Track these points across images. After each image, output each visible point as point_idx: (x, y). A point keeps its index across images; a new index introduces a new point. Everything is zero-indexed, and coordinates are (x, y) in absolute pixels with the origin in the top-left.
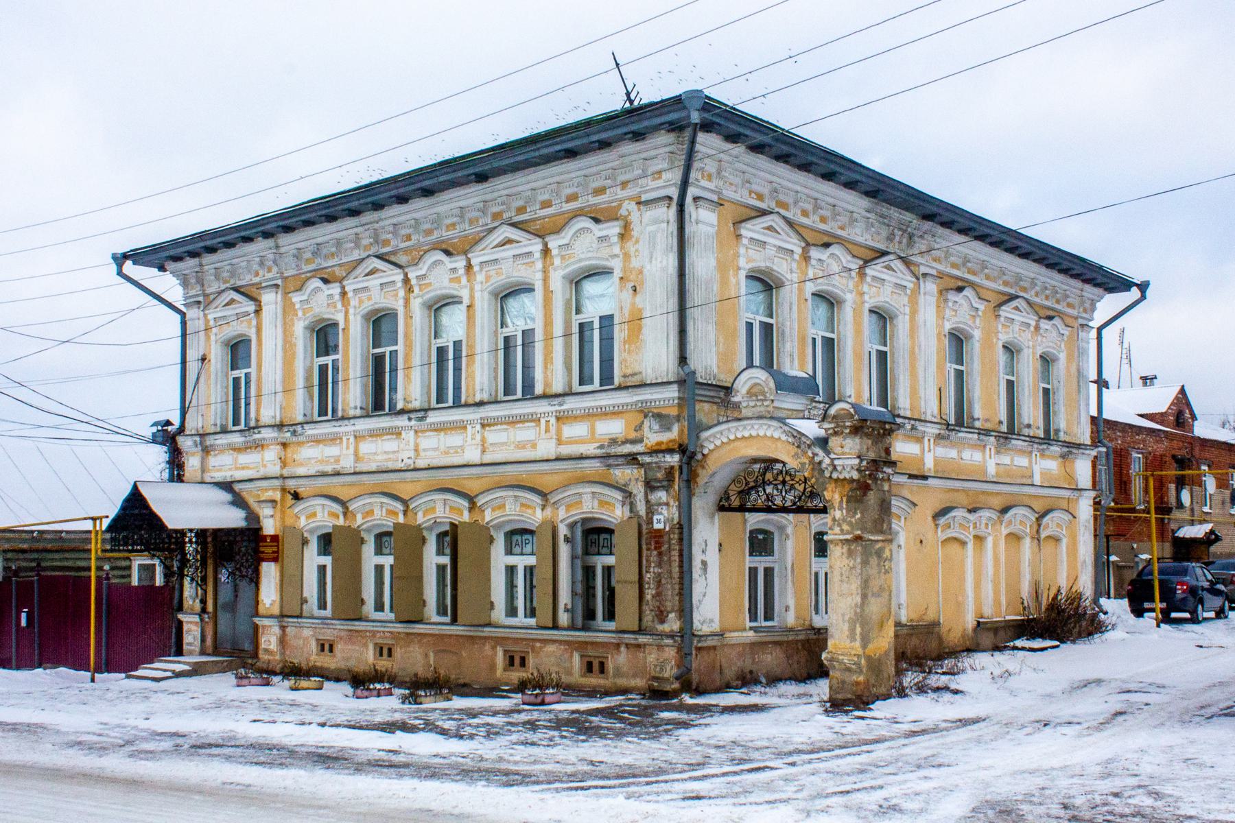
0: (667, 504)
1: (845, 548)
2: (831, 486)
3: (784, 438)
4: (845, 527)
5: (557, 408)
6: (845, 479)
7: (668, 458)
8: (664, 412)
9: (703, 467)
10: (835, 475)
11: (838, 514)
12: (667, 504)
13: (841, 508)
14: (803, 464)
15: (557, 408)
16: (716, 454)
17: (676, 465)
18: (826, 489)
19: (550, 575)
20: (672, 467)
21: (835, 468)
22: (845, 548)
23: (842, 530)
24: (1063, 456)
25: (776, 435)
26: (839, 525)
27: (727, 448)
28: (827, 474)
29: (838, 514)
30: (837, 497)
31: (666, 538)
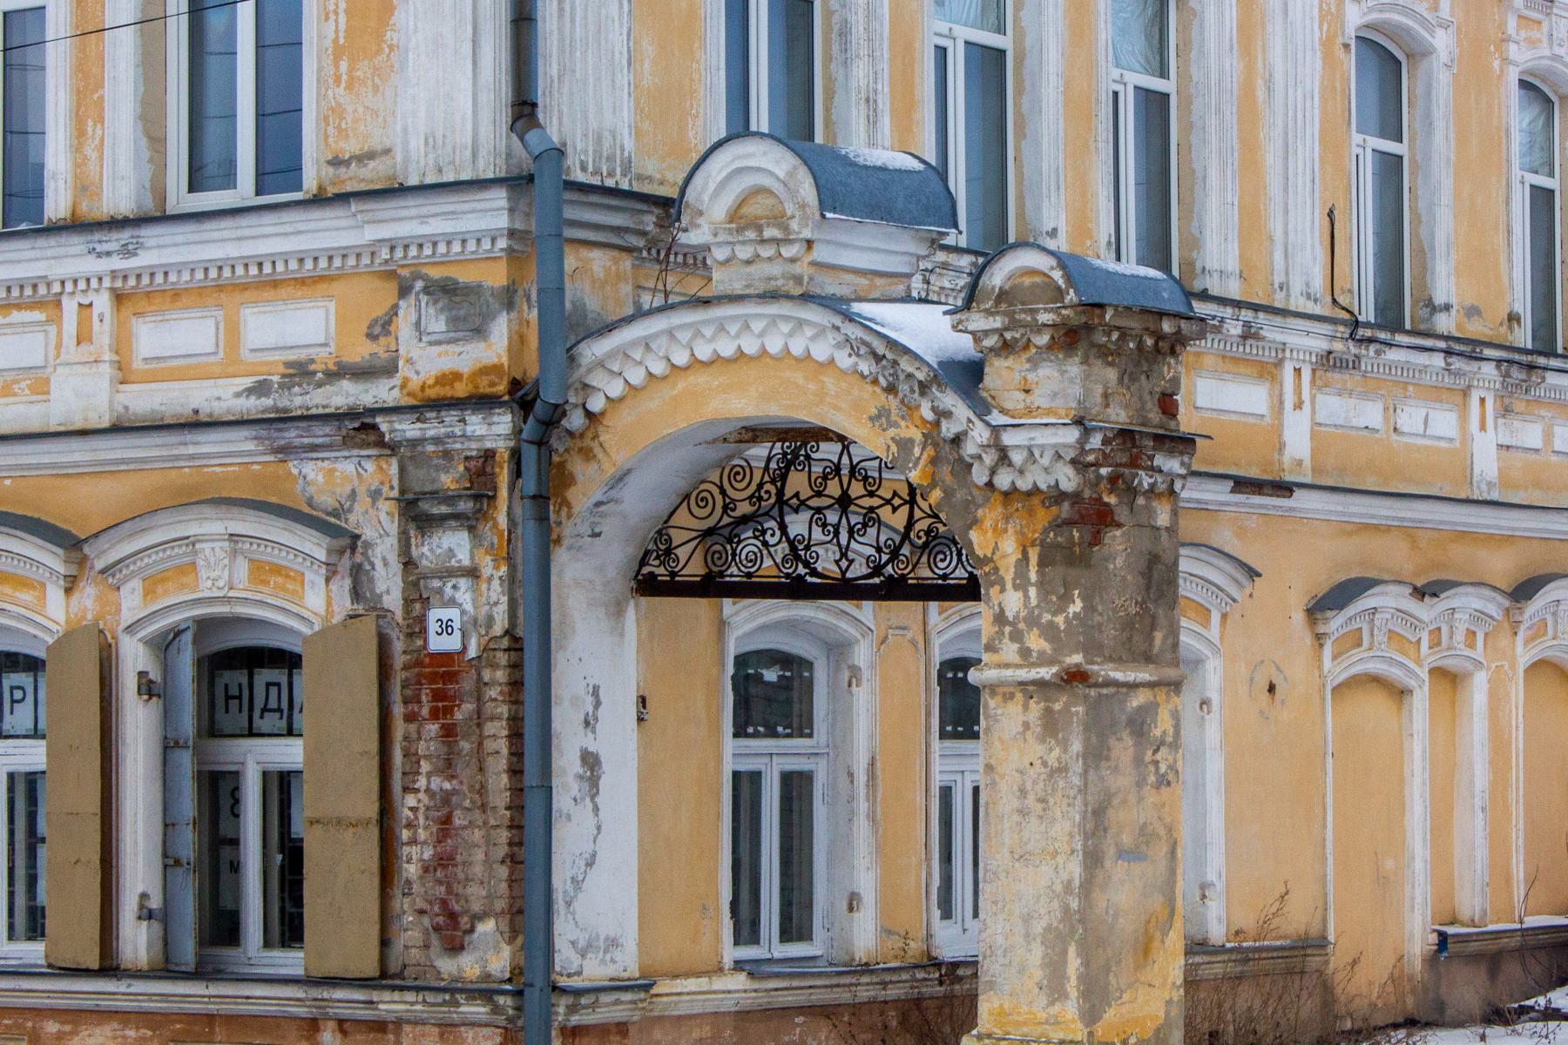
0: (473, 573)
1: (1036, 708)
2: (990, 514)
3: (844, 360)
4: (1036, 642)
5: (117, 263)
6: (1035, 491)
10: (1004, 480)
12: (473, 573)
13: (1021, 584)
14: (905, 445)
15: (117, 263)
17: (502, 446)
18: (975, 522)
20: (489, 455)
22: (1036, 708)
23: (1025, 652)
25: (821, 351)
26: (1017, 636)
29: (1013, 602)
30: (1009, 547)
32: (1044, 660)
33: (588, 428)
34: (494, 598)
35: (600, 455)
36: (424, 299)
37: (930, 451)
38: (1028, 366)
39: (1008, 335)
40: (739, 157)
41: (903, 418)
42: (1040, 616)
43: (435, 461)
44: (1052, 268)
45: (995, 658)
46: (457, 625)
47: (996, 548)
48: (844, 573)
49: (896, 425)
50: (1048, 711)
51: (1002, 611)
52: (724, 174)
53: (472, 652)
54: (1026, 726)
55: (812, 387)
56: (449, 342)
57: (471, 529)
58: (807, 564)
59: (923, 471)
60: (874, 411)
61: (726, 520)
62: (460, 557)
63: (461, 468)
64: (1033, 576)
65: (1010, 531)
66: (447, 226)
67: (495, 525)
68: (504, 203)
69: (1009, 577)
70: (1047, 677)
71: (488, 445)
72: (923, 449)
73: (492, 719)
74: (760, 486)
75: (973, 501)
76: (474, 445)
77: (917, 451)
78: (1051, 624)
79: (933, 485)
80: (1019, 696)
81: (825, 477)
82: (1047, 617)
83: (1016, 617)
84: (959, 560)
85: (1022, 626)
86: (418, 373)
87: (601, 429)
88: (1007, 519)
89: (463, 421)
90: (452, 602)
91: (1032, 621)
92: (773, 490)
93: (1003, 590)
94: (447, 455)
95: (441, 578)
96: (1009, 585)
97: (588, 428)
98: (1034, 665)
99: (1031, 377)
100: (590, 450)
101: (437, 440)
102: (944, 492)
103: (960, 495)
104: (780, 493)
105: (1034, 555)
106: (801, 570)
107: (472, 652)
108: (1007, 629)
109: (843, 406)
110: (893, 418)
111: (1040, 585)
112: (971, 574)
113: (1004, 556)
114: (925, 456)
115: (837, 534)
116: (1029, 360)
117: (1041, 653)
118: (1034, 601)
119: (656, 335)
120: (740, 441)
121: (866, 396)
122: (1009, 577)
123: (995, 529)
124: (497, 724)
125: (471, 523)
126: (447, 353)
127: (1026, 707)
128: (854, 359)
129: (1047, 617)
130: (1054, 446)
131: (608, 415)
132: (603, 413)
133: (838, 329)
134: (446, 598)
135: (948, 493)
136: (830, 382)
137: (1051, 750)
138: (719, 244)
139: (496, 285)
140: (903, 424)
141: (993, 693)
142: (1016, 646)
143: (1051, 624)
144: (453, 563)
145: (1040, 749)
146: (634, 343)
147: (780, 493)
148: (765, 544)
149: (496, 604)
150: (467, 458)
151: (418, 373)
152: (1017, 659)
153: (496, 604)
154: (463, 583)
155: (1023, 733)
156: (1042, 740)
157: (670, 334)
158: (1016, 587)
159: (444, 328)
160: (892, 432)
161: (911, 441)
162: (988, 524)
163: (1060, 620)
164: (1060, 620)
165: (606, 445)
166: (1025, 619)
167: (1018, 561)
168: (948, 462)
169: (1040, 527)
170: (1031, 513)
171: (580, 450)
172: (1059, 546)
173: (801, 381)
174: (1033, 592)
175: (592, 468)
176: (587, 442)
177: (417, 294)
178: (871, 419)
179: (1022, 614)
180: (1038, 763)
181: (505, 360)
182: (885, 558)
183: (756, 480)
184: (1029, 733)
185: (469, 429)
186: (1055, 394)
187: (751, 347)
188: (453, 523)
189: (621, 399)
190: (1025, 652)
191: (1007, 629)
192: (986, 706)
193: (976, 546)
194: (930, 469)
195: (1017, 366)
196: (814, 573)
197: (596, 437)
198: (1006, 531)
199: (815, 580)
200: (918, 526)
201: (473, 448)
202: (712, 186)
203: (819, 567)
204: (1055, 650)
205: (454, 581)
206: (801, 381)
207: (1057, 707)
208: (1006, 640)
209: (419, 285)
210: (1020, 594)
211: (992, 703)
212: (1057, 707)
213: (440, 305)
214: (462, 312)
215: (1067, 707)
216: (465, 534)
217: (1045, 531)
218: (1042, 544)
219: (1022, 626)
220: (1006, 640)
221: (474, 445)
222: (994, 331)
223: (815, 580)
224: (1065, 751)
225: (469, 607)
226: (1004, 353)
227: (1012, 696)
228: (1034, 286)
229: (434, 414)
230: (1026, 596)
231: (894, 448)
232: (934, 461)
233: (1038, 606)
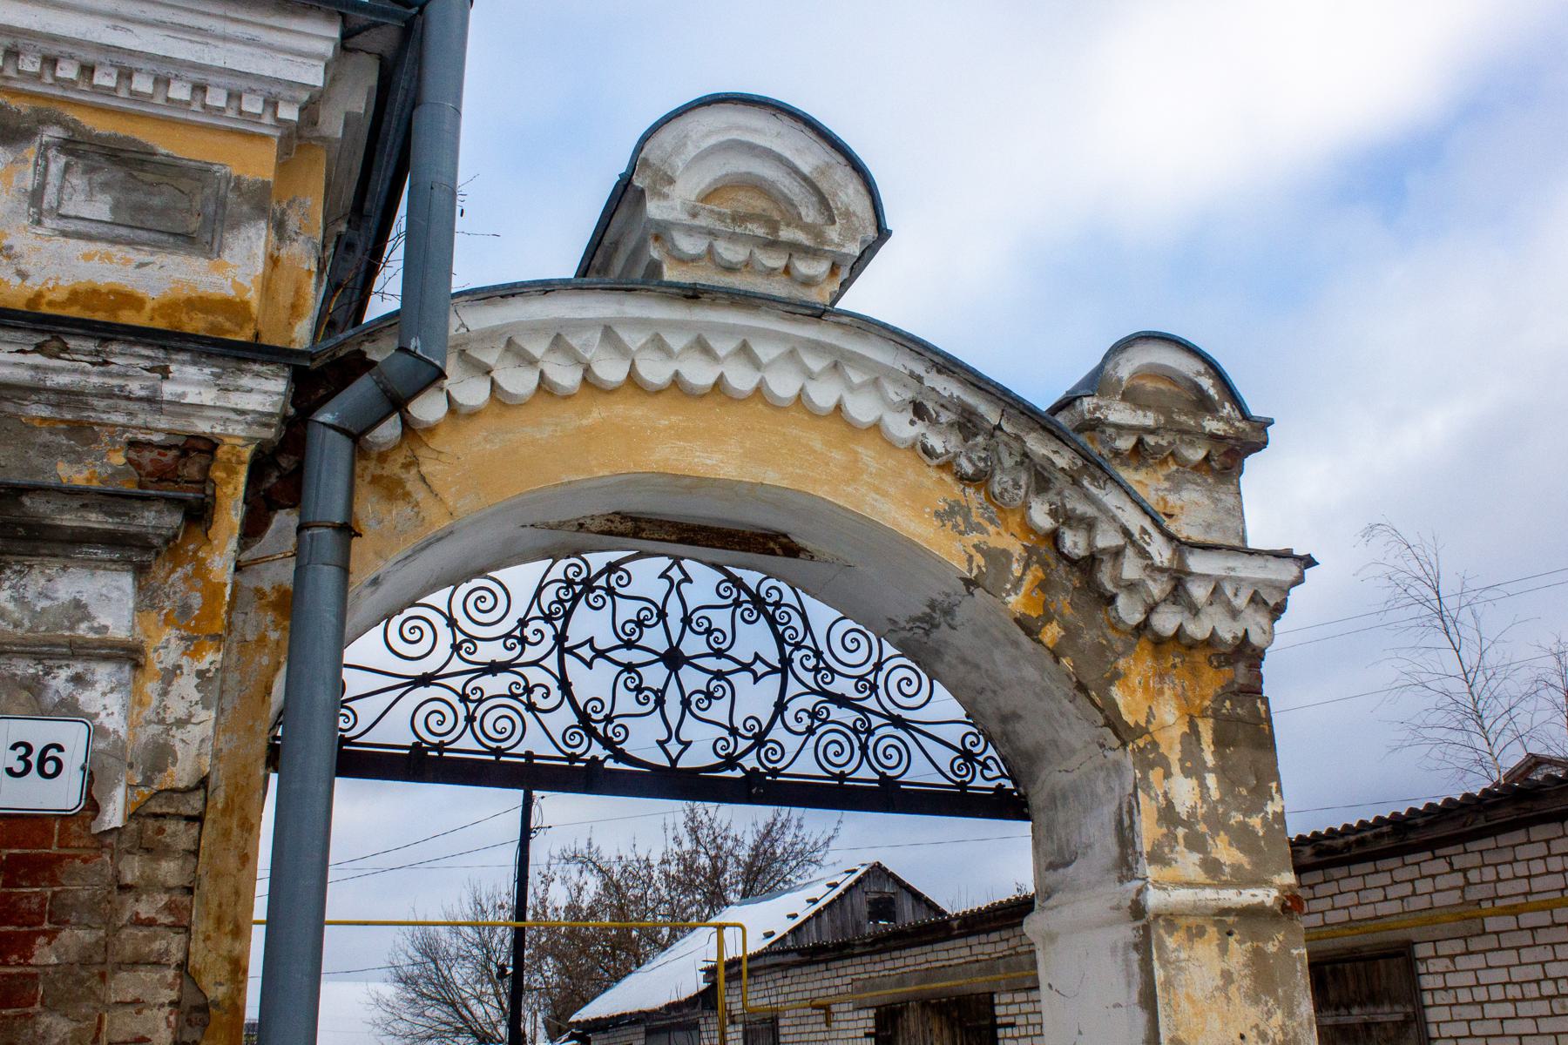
0: (130, 655)
1: (1238, 952)
2: (1138, 667)
3: (903, 428)
4: (1226, 853)
6: (1212, 641)
7: (191, 383)
8: (165, 144)
9: (392, 490)
10: (1167, 621)
11: (1184, 793)
12: (130, 655)
13: (1194, 770)
14: (998, 559)
16: (475, 444)
17: (239, 439)
18: (1116, 676)
19: (396, 928)
20: (207, 446)
21: (1179, 579)
22: (1238, 952)
23: (1212, 867)
24: (49, 943)
25: (863, 409)
26: (1196, 843)
27: (569, 419)
28: (1129, 611)
29: (1184, 793)
30: (1169, 715)
31: (80, 886)
32: (1242, 880)
33: (398, 447)
34: (177, 709)
35: (420, 494)
36: (57, 163)
37: (1035, 572)
38: (1166, 485)
39: (1151, 440)
40: (739, 128)
41: (991, 521)
42: (1226, 814)
43: (46, 437)
44: (1199, 373)
45: (1167, 873)
46: (74, 758)
47: (1151, 715)
48: (674, 762)
49: (979, 528)
50: (1258, 956)
51: (1170, 805)
52: (712, 141)
53: (114, 815)
54: (1227, 976)
55: (837, 455)
56: (114, 241)
57: (140, 570)
58: (607, 743)
59: (1028, 596)
60: (942, 506)
61: (457, 665)
62: (103, 619)
63: (119, 459)
64: (1210, 759)
65: (1168, 693)
66: (182, 49)
67: (201, 569)
68: (327, 49)
69: (1174, 757)
70: (1269, 902)
71: (203, 427)
72: (1026, 567)
73: (135, 963)
74: (523, 623)
75: (1110, 646)
76: (163, 423)
77: (1017, 569)
78: (1244, 826)
79: (1048, 618)
80: (1212, 931)
81: (640, 623)
82: (1236, 818)
83: (1192, 813)
84: (864, 753)
85: (1202, 828)
86: (23, 275)
87: (422, 453)
88: (1161, 676)
89: (165, 373)
90: (68, 710)
91: (1217, 823)
92: (549, 631)
93: (1168, 775)
94: (79, 429)
95: (38, 658)
96: (1176, 768)
97: (398, 447)
98: (1226, 885)
99: (1171, 498)
100: (400, 483)
101: (69, 397)
102: (1065, 628)
103: (1088, 637)
104: (560, 638)
105: (1206, 729)
106: (598, 751)
107: (114, 815)
108: (1181, 832)
109: (892, 490)
110: (975, 518)
111: (1222, 771)
112: (882, 775)
113: (1163, 727)
114: (1029, 577)
115: (660, 702)
116: (1168, 478)
117: (1236, 868)
118: (1215, 794)
119: (582, 325)
120: (610, 533)
121: (928, 483)
122: (1174, 757)
123: (1146, 689)
124: (147, 975)
125: (135, 553)
126: (109, 257)
127: (1224, 950)
128: (920, 427)
129: (1236, 818)
130: (1254, 582)
131: (442, 432)
132: (431, 430)
133: (919, 379)
134: (50, 698)
135: (1071, 633)
136: (868, 454)
137: (1269, 1014)
138: (690, 230)
139: (248, 176)
140: (991, 529)
141: (1171, 926)
142: (1196, 857)
143: (1244, 826)
144: (82, 630)
145: (1253, 1013)
146: (535, 329)
147: (560, 638)
148: (531, 707)
149: (181, 723)
150: (133, 444)
151: (23, 275)
152: (1197, 874)
153: (181, 723)
154: (103, 673)
155: (1224, 989)
156: (1255, 1000)
157: (608, 332)
158: (1187, 773)
159: (106, 216)
160: (975, 538)
161: (1006, 554)
162: (1135, 680)
163: (1256, 821)
164: (1256, 821)
165: (436, 484)
166: (1205, 818)
167: (1184, 735)
168: (1067, 592)
169: (1210, 692)
170: (1194, 671)
171: (376, 480)
172: (1240, 720)
173: (818, 445)
174: (1211, 780)
175: (399, 512)
176: (393, 468)
177: (46, 147)
178: (937, 514)
179: (1201, 811)
180: (1252, 1036)
181: (253, 296)
182: (743, 745)
183: (518, 612)
184: (1233, 989)
185: (168, 390)
186: (1209, 526)
187: (741, 379)
188: (101, 554)
189: (473, 414)
190: (1212, 867)
191: (1181, 832)
192: (1161, 947)
193: (1122, 710)
194: (1037, 594)
195: (1152, 483)
196: (620, 756)
197: (413, 463)
198: (1161, 692)
199: (621, 766)
200: (793, 707)
201: (161, 425)
202: (691, 151)
203: (628, 747)
204: (1255, 864)
205: (78, 667)
206: (818, 445)
207: (1271, 948)
208: (1180, 848)
209: (52, 133)
210: (1193, 782)
211: (1171, 942)
212: (1271, 948)
213: (99, 178)
214: (156, 201)
215: (1285, 949)
216: (126, 581)
217: (1219, 699)
218: (1216, 714)
219: (1202, 828)
220: (1180, 848)
221: (163, 423)
222: (1131, 429)
223: (621, 766)
224: (1290, 1014)
225: (114, 721)
226: (1134, 463)
227: (1201, 932)
228: (1158, 392)
229: (91, 345)
230: (1203, 785)
231: (979, 560)
232: (1044, 586)
233: (1221, 801)
